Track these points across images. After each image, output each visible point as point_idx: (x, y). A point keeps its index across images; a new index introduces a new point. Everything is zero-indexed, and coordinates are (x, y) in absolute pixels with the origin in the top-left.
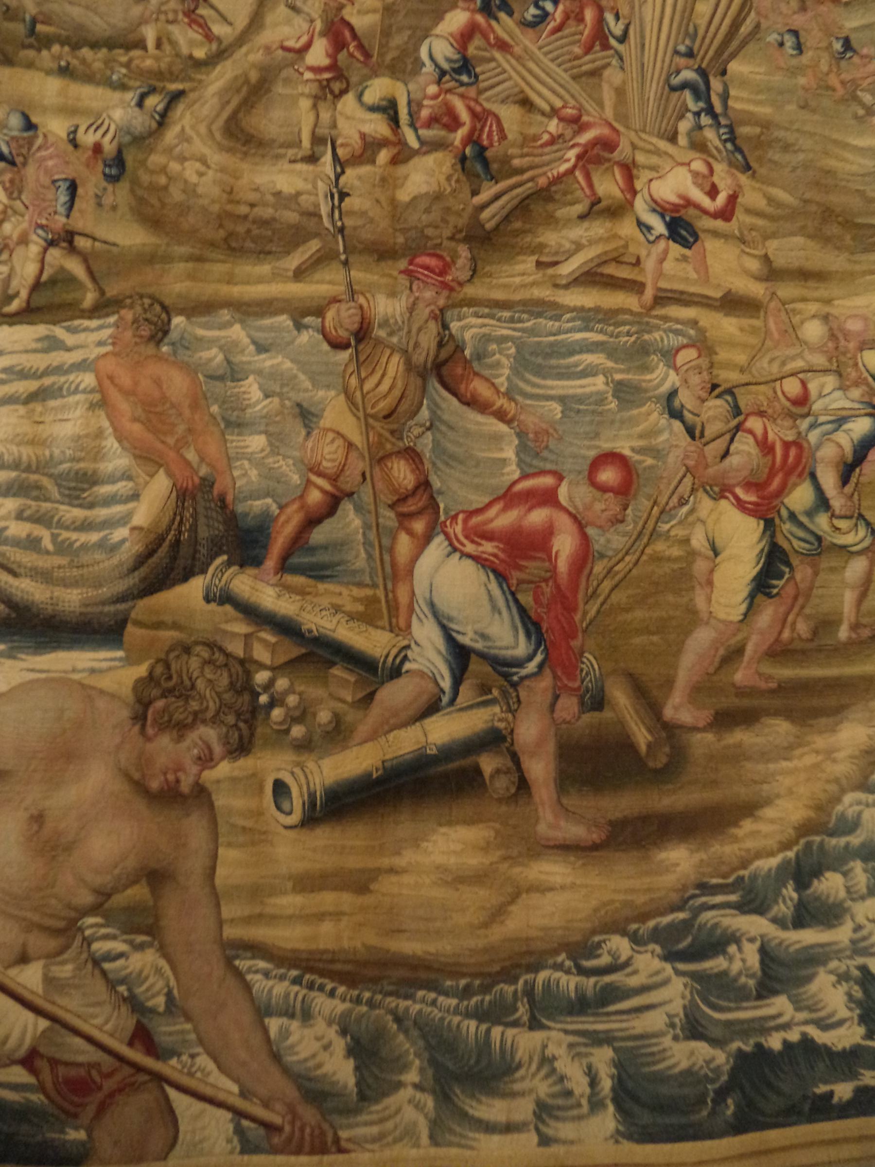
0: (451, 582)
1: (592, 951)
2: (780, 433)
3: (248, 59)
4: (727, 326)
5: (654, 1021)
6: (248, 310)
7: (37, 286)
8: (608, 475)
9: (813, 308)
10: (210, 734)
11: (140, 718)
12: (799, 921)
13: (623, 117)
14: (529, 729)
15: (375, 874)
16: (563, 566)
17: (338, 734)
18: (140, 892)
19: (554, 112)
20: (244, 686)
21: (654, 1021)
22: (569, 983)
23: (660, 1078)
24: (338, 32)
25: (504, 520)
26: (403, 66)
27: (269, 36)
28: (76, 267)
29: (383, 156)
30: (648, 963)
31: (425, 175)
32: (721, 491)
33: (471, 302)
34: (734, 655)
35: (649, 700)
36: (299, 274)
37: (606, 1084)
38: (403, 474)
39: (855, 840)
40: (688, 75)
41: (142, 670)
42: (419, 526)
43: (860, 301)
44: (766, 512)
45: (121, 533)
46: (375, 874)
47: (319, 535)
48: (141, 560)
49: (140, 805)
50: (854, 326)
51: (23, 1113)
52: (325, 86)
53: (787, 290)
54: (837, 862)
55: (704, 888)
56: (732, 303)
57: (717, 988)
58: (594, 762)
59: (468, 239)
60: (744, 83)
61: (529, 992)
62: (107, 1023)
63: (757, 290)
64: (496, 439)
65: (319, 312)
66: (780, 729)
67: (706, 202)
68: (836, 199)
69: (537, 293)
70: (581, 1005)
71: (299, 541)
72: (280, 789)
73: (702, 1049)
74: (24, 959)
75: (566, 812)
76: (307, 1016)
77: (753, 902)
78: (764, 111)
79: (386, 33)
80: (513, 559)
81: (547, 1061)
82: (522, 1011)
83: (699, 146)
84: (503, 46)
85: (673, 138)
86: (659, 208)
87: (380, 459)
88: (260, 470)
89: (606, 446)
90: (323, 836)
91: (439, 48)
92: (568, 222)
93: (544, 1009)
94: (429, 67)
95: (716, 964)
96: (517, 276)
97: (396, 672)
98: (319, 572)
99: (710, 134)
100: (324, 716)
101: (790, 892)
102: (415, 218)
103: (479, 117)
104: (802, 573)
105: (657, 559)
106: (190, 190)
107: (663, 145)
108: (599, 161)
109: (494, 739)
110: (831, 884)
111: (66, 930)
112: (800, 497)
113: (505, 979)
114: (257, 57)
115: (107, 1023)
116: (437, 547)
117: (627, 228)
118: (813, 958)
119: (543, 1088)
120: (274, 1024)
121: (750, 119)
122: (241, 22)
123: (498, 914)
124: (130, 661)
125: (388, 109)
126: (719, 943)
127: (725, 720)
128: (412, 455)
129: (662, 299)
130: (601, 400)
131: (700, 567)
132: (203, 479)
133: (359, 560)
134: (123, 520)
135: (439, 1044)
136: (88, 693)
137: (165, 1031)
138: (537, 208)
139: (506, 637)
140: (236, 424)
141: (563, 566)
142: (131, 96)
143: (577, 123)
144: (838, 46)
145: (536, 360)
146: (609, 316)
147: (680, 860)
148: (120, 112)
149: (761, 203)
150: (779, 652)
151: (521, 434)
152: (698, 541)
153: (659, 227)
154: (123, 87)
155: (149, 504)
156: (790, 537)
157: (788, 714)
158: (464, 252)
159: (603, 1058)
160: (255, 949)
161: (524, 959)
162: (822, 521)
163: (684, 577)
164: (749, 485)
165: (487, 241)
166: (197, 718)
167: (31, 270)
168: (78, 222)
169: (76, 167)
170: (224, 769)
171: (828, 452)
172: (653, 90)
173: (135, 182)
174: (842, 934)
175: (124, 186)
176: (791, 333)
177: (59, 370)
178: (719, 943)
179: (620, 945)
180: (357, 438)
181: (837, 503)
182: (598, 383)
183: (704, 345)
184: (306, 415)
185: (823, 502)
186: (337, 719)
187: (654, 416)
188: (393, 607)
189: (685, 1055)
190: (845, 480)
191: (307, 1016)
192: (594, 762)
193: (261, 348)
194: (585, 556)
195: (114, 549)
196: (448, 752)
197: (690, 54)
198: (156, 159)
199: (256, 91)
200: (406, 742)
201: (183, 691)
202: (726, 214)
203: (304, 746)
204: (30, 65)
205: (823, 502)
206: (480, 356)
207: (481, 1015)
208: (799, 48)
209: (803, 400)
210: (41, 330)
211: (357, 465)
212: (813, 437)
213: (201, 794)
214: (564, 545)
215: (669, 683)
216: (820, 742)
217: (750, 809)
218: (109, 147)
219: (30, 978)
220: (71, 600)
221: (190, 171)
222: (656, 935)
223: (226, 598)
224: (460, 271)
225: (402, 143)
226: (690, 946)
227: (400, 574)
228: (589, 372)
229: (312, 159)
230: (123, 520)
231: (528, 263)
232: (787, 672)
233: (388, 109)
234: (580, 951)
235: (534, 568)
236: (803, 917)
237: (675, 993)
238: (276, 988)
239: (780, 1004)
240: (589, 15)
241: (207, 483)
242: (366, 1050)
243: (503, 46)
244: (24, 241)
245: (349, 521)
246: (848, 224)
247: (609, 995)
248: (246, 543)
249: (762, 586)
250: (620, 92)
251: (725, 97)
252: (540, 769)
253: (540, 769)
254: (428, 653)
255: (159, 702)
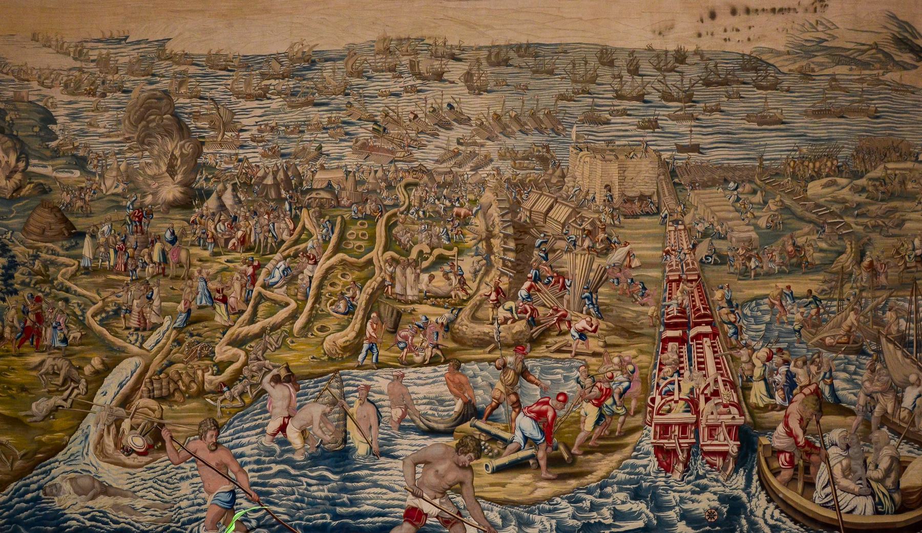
0: (526, 424)
1: (553, 500)
2: (605, 386)
3: (477, 298)
4: (593, 360)
5: (565, 515)
6: (478, 361)
7: (431, 358)
8: (561, 398)
9: (616, 354)
10: (472, 455)
11: (457, 451)
12: (600, 497)
13: (568, 308)
14: (541, 454)
15: (506, 484)
16: (550, 419)
17: (499, 455)
18: (458, 486)
19: (551, 308)
20: (479, 445)
21: (565, 515)
22: (547, 507)
23: (566, 526)
24: (498, 290)
25: (536, 408)
26: (515, 298)
27: (481, 292)
28: (439, 353)
29: (509, 322)
30: (564, 503)
31: (520, 326)
32: (589, 400)
33: (530, 357)
34: (589, 439)
35: (568, 448)
36: (490, 352)
37: (554, 527)
38: (513, 398)
39: (615, 480)
40: (587, 294)
41: (457, 441)
42: (517, 410)
43: (628, 352)
44: (599, 404)
45: (451, 413)
46: (506, 484)
47: (495, 412)
48: (456, 419)
49: (458, 469)
50: (627, 358)
51: (437, 526)
52: (495, 305)
53: (609, 350)
54: (611, 485)
55: (578, 489)
56: (595, 354)
57: (581, 509)
58: (554, 461)
59: (529, 342)
60: (602, 294)
61: (538, 508)
62: (453, 511)
63: (602, 350)
64: (535, 390)
65: (494, 361)
66: (599, 455)
67: (590, 329)
68: (625, 325)
69: (546, 354)
70: (550, 511)
71: (490, 413)
72: (487, 466)
73: (575, 522)
74: (435, 498)
75: (549, 473)
76: (492, 511)
77: (590, 492)
78: (607, 301)
79: (510, 290)
80: (539, 416)
81: (542, 522)
82: (537, 512)
83: (589, 314)
84: (539, 291)
85: (582, 312)
86: (578, 331)
87: (508, 395)
88: (482, 398)
89: (561, 391)
90: (495, 476)
91: (523, 293)
92: (554, 336)
93: (542, 512)
94: (520, 298)
95: (580, 504)
96: (541, 350)
97: (511, 442)
98: (495, 420)
99: (592, 310)
100: (496, 451)
101: (599, 490)
102: (516, 337)
103: (533, 310)
104: (608, 420)
105: (572, 417)
106: (464, 333)
107: (580, 315)
108: (562, 320)
109: (533, 456)
110: (608, 490)
111: (444, 493)
112: (609, 402)
113: (532, 504)
114: (479, 298)
115: (453, 511)
116: (521, 414)
117: (569, 337)
118: (603, 505)
119: (541, 527)
120: (485, 512)
121: (604, 304)
122: (475, 289)
123: (532, 492)
124: (455, 439)
125: (510, 310)
126: (581, 500)
127: (585, 453)
128: (516, 394)
129: (577, 354)
130: (560, 380)
131: (582, 419)
132: (56, 120)
133: (504, 417)
134: (453, 410)
135: (519, 518)
136: (446, 446)
137: (463, 512)
138: (546, 333)
139: (536, 434)
140: (476, 387)
141: (550, 419)
142: (449, 311)
143: (557, 311)
144: (629, 281)
145: (545, 371)
146: (563, 360)
147: (573, 483)
148: (447, 314)
149: (604, 327)
150: (600, 438)
151: (541, 388)
152: (582, 413)
153: (577, 336)
154: (447, 308)
155: (458, 406)
156: (606, 411)
157: (601, 452)
158: (528, 345)
159: (554, 522)
160: (482, 498)
161: (537, 502)
162: (614, 407)
163: (578, 421)
164: (595, 399)
165: (535, 342)
166: (469, 452)
167: (429, 354)
168: (440, 342)
169: (438, 329)
170: (475, 462)
171: (617, 391)
172: (577, 299)
173: (452, 332)
174: (610, 500)
175: (449, 333)
176: (610, 361)
177: (437, 377)
178: (581, 500)
179: (559, 500)
180: (503, 391)
181: (618, 403)
182: (559, 376)
183: (587, 366)
184: (492, 386)
185: (615, 403)
186: (499, 452)
187: (573, 383)
188: (511, 428)
189: (571, 522)
190: (620, 397)
191: (492, 511)
192: (554, 461)
193: (481, 370)
194: (555, 416)
195: (450, 416)
196: (522, 459)
197: (588, 288)
198: (456, 326)
199: (478, 306)
200: (514, 457)
201: (466, 446)
202: (595, 331)
203: (492, 457)
204: (426, 303)
205: (615, 403)
206: (532, 370)
207: (528, 512)
208: (618, 283)
209: (612, 378)
210: (433, 367)
211: (503, 396)
212: (614, 387)
213: (470, 467)
214: (550, 414)
215: (573, 445)
216: (608, 458)
217: (591, 473)
218: (445, 323)
219: (437, 502)
220: (441, 427)
221: (464, 328)
222: (566, 498)
223: (475, 426)
224: (527, 350)
225: (514, 318)
226: (574, 500)
227: (513, 420)
228: (558, 374)
229: (492, 324)
230: (453, 410)
231: (544, 347)
232: (602, 443)
233: (510, 310)
234: (550, 500)
235: (543, 419)
236: (601, 496)
237: (571, 510)
238: (485, 505)
239: (594, 514)
240: (561, 280)
241: (470, 401)
242: (504, 518)
243: (539, 291)
244: (428, 347)
245: (502, 409)
246: (628, 332)
247: (555, 510)
248: (479, 414)
249: (597, 423)
250: (568, 301)
251: (597, 299)
252: (543, 463)
253: (543, 463)
254: (519, 438)
255: (461, 448)
